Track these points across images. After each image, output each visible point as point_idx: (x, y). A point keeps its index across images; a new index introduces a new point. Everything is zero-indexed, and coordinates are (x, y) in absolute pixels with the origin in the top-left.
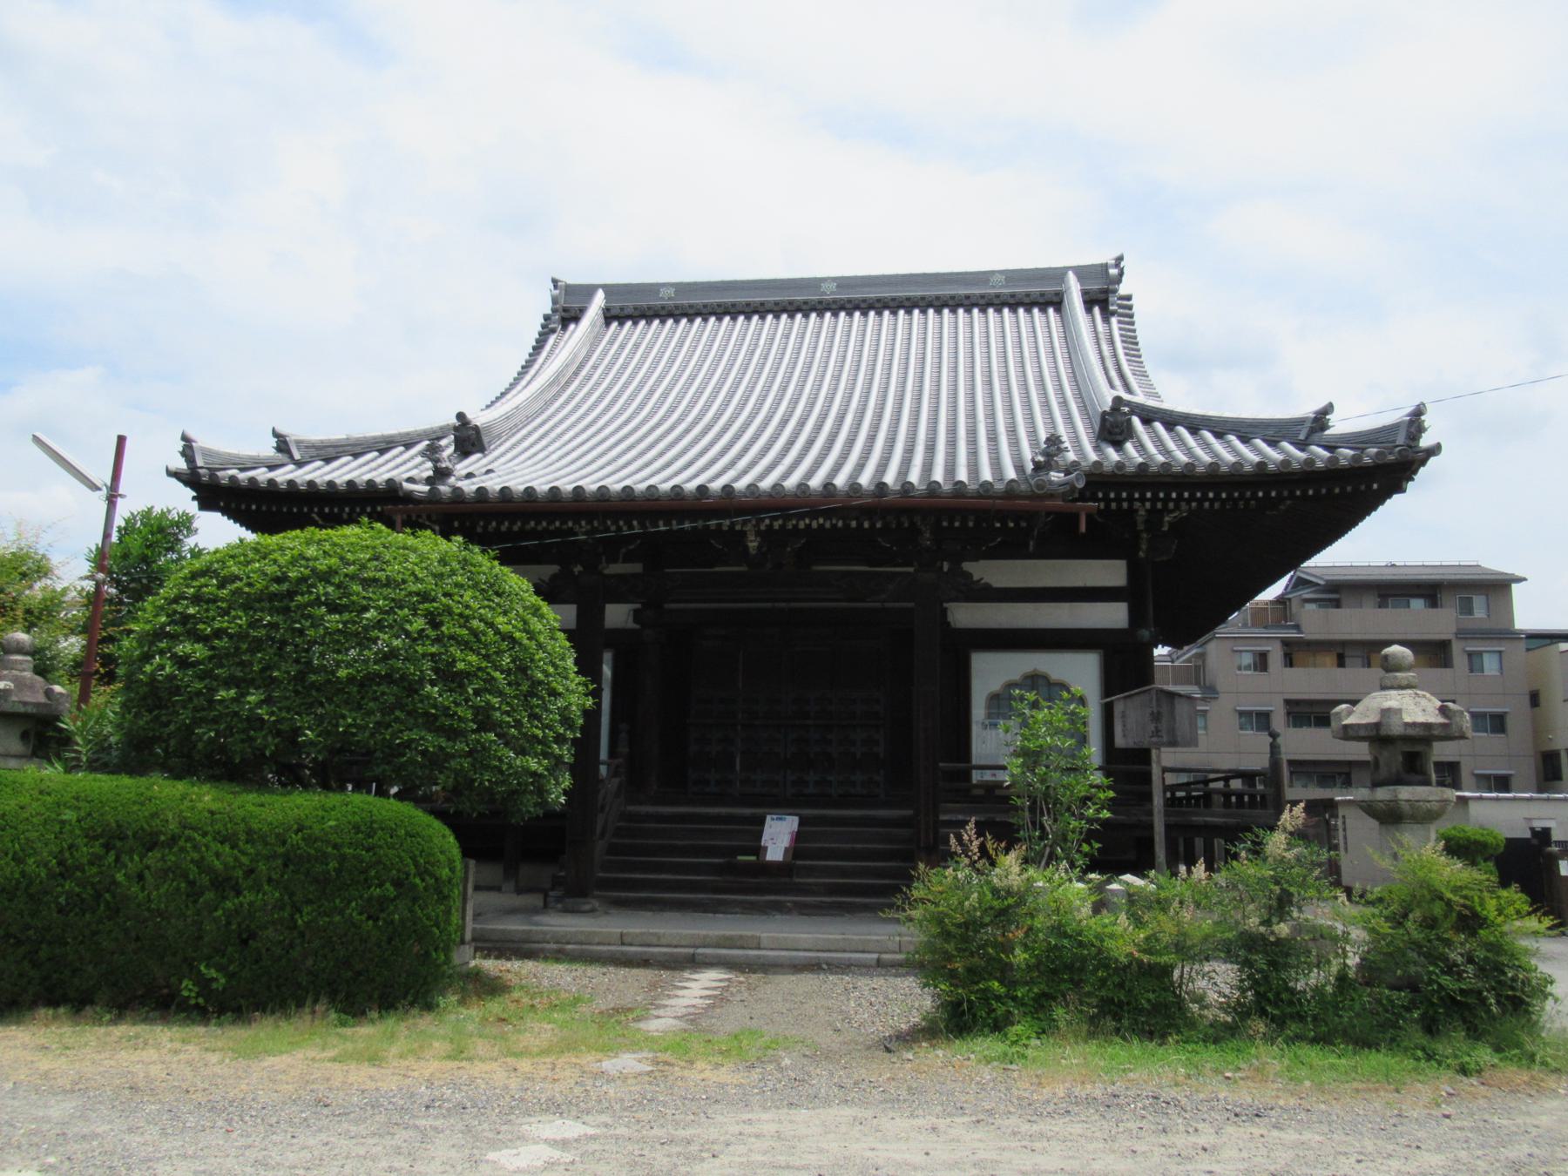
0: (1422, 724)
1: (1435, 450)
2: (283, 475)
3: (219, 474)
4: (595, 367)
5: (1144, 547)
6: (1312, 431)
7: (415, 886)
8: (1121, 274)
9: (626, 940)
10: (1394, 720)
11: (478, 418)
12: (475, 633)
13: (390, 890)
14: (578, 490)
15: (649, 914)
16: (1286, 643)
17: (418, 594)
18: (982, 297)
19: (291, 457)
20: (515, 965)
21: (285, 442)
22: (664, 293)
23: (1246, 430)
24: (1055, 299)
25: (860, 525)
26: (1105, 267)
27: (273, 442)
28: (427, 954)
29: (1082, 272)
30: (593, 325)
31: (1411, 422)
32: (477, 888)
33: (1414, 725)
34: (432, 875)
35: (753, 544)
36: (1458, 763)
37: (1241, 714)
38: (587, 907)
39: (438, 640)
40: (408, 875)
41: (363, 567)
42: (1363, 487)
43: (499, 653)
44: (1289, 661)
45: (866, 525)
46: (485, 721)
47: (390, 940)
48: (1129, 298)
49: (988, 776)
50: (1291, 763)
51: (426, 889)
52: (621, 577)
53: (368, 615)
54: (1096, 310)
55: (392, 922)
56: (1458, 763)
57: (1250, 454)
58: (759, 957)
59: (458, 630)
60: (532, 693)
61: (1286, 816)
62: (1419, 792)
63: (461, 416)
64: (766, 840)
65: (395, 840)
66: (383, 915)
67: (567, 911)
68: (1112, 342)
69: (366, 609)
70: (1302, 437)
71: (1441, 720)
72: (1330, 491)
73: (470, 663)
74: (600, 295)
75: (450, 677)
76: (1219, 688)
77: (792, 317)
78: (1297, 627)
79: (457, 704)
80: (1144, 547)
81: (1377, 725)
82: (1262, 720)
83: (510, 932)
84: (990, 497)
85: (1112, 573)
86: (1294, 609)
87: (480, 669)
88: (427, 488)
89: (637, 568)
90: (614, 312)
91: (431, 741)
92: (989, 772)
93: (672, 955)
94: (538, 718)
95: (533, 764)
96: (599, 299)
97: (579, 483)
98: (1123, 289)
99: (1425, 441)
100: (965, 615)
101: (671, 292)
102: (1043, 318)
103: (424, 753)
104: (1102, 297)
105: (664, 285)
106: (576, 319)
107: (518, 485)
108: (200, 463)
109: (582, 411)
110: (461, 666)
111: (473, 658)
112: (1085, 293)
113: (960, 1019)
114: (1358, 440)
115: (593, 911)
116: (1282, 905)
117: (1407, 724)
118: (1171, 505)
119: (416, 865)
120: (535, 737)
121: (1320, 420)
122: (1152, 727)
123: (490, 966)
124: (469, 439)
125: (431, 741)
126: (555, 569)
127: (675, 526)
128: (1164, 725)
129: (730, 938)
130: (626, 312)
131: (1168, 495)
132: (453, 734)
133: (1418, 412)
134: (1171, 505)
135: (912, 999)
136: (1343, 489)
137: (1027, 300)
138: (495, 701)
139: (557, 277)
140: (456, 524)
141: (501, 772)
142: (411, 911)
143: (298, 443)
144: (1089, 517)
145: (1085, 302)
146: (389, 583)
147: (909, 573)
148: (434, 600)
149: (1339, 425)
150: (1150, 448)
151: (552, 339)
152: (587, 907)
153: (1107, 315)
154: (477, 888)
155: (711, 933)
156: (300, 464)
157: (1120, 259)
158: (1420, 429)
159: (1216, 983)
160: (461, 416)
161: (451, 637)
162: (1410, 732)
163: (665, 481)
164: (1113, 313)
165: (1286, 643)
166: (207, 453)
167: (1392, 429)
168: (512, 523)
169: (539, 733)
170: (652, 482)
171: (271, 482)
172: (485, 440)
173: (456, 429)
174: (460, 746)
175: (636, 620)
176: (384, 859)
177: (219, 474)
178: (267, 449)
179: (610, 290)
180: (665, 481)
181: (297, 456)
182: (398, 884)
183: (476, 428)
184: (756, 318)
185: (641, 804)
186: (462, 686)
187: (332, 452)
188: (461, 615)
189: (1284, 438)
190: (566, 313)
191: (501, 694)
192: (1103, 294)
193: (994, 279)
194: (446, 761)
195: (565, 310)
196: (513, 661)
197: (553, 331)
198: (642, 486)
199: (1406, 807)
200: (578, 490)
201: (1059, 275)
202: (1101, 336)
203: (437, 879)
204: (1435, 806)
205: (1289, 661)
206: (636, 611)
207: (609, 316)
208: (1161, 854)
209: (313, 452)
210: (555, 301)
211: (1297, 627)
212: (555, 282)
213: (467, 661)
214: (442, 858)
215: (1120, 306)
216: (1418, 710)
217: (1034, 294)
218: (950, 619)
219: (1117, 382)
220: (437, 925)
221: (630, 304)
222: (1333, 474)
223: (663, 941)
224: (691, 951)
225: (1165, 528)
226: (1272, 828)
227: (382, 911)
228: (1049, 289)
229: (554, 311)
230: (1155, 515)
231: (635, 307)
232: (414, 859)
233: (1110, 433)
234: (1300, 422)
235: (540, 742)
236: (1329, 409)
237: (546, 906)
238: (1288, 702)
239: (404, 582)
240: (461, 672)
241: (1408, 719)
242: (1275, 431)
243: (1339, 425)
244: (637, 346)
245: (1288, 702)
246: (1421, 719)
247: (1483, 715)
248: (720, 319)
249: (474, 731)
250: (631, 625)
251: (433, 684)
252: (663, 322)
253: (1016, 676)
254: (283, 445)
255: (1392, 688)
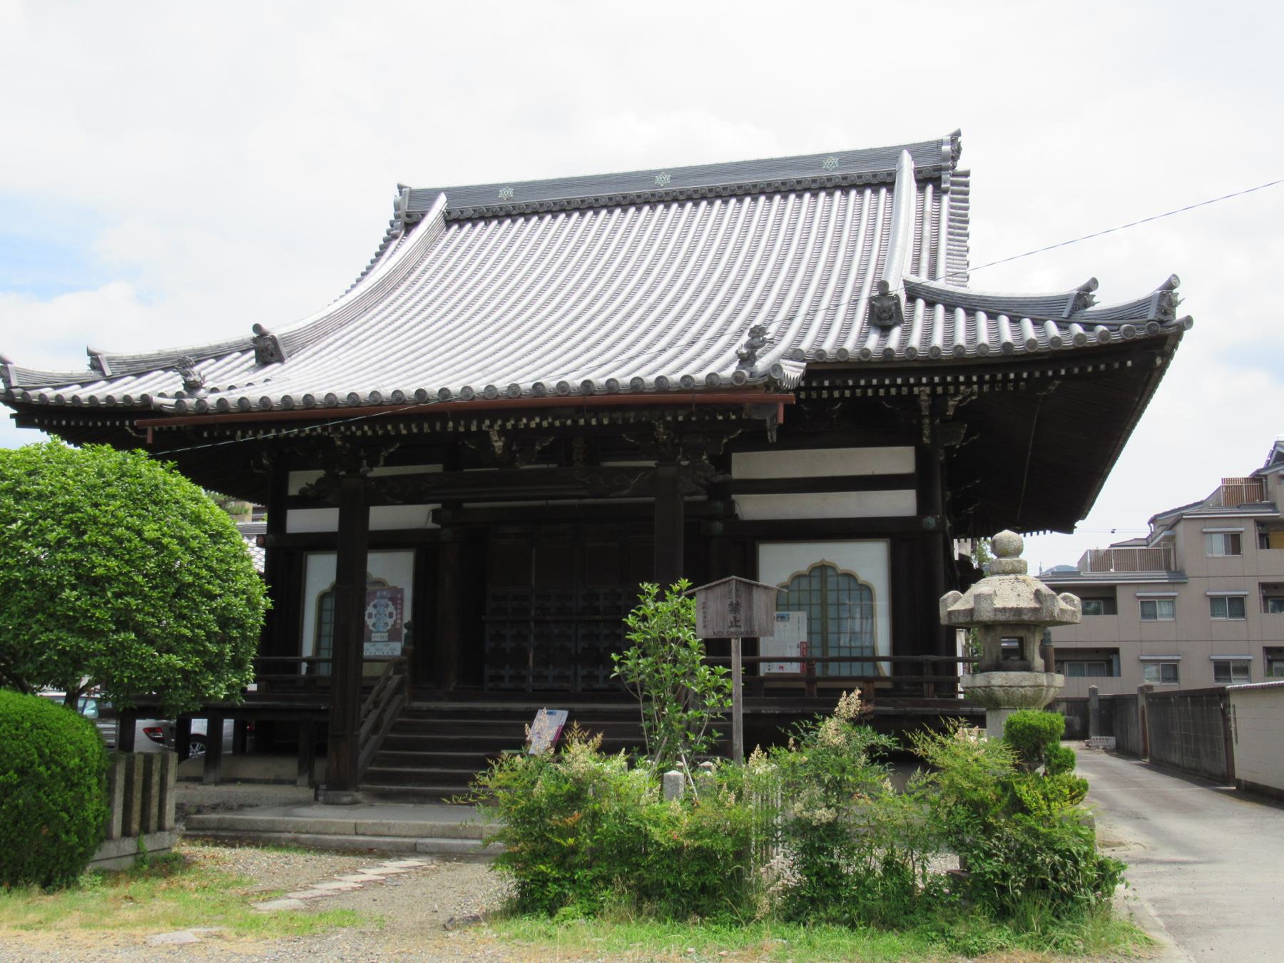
0: (1011, 609)
1: (1188, 321)
2: (101, 391)
3: (30, 393)
4: (424, 272)
5: (927, 432)
6: (1075, 309)
7: (38, 775)
8: (958, 151)
9: (361, 830)
10: (985, 605)
11: (276, 329)
12: (120, 540)
13: (13, 777)
14: (562, 386)
15: (411, 806)
16: (1260, 523)
17: (63, 505)
18: (814, 181)
19: (104, 374)
20: (209, 850)
21: (98, 360)
22: (503, 194)
23: (1015, 310)
24: (889, 180)
25: (575, 422)
26: (940, 143)
27: (88, 360)
28: (56, 837)
29: (917, 151)
30: (431, 229)
31: (1162, 296)
32: (179, 780)
33: (1004, 610)
34: (58, 764)
35: (498, 444)
36: (1116, 651)
37: (1215, 600)
38: (346, 799)
39: (81, 547)
40: (32, 763)
41: (19, 483)
42: (1116, 365)
43: (144, 558)
44: (1265, 541)
45: (594, 422)
46: (123, 621)
47: (15, 823)
48: (967, 174)
49: (775, 668)
50: (1058, 651)
51: (52, 776)
52: (381, 480)
53: (14, 526)
54: (930, 188)
55: (17, 806)
56: (1116, 651)
57: (989, 334)
58: (350, 842)
59: (101, 539)
60: (178, 594)
61: (842, 703)
62: (1013, 677)
63: (257, 328)
64: (531, 733)
65: (20, 732)
66: (8, 800)
67: (328, 803)
68: (937, 222)
69: (14, 520)
70: (1065, 315)
71: (1033, 605)
72: (1083, 369)
73: (109, 569)
74: (442, 199)
75: (92, 583)
76: (1188, 573)
77: (770, 198)
78: (1273, 506)
79: (95, 606)
80: (927, 432)
81: (971, 611)
82: (1236, 606)
83: (256, 822)
84: (691, 391)
85: (900, 460)
86: (1270, 488)
87: (121, 574)
88: (174, 401)
89: (437, 468)
90: (454, 216)
91: (70, 641)
92: (776, 665)
93: (395, 844)
94: (184, 617)
95: (177, 661)
96: (441, 203)
97: (612, 376)
98: (961, 166)
99: (1180, 314)
100: (752, 508)
101: (510, 192)
102: (859, 201)
103: (63, 653)
104: (936, 174)
105: (504, 185)
106: (416, 224)
107: (297, 394)
108: (14, 383)
109: (553, 304)
110: (100, 571)
111: (113, 563)
112: (918, 172)
113: (533, 901)
114: (1115, 316)
115: (354, 803)
116: (838, 789)
117: (997, 610)
118: (952, 389)
119: (41, 755)
120: (184, 636)
121: (1083, 297)
122: (730, 617)
123: (186, 849)
124: (267, 350)
125: (70, 641)
126: (319, 474)
127: (261, 436)
128: (742, 615)
129: (454, 829)
130: (466, 215)
131: (1006, 376)
132: (91, 634)
133: (1170, 286)
134: (952, 389)
135: (490, 885)
136: (1096, 367)
137: (859, 182)
138: (133, 602)
139: (404, 183)
140: (205, 435)
141: (144, 670)
142: (35, 797)
143: (110, 360)
144: (787, 407)
145: (918, 181)
146: (40, 496)
147: (650, 468)
148: (79, 510)
149: (1104, 300)
150: (926, 332)
151: (395, 243)
152: (346, 799)
153: (939, 192)
154: (179, 780)
155: (437, 823)
156: (110, 380)
157: (958, 134)
158: (1173, 304)
159: (781, 868)
160: (257, 328)
161: (95, 544)
162: (1001, 617)
163: (699, 370)
164: (945, 192)
165: (1260, 523)
166: (22, 373)
167: (1143, 304)
168: (531, 419)
169: (188, 633)
170: (711, 369)
171: (59, 397)
172: (284, 351)
173: (254, 340)
174: (98, 646)
175: (434, 521)
176: (8, 749)
177: (30, 393)
178: (82, 366)
179: (452, 193)
180: (699, 370)
181: (108, 373)
182: (21, 771)
183: (273, 339)
184: (748, 200)
185: (439, 699)
186: (104, 590)
187: (142, 367)
188: (105, 525)
189: (1050, 316)
190: (407, 221)
191: (145, 598)
192: (939, 172)
193: (827, 163)
194: (86, 659)
195: (408, 216)
196: (159, 566)
197: (395, 237)
198: (677, 377)
199: (1000, 693)
200: (587, 384)
201: (892, 155)
202: (927, 216)
203: (64, 768)
204: (1030, 692)
205: (1265, 541)
206: (434, 512)
207: (451, 220)
208: (738, 742)
209: (124, 368)
210: (397, 207)
211: (1273, 506)
212: (400, 187)
213: (103, 565)
214: (70, 748)
215: (953, 184)
216: (1013, 595)
217: (867, 176)
218: (737, 511)
219: (925, 264)
220: (67, 810)
221: (469, 207)
222: (1104, 351)
223: (393, 832)
224: (413, 840)
225: (950, 413)
226: (830, 714)
227: (6, 796)
228: (881, 169)
229: (397, 217)
230: (938, 401)
231: (475, 209)
232: (39, 749)
233: (880, 319)
234: (1061, 300)
235: (189, 640)
236: (1093, 284)
237: (316, 799)
238: (1263, 586)
239: (52, 493)
240: (101, 578)
241: (999, 604)
242: (1038, 310)
243: (1104, 300)
244: (614, 231)
245: (1263, 586)
246: (1012, 604)
247: (1222, 598)
248: (740, 201)
249: (114, 632)
250: (431, 525)
251: (73, 588)
252: (625, 211)
253: (803, 568)
254: (96, 364)
255: (998, 573)
